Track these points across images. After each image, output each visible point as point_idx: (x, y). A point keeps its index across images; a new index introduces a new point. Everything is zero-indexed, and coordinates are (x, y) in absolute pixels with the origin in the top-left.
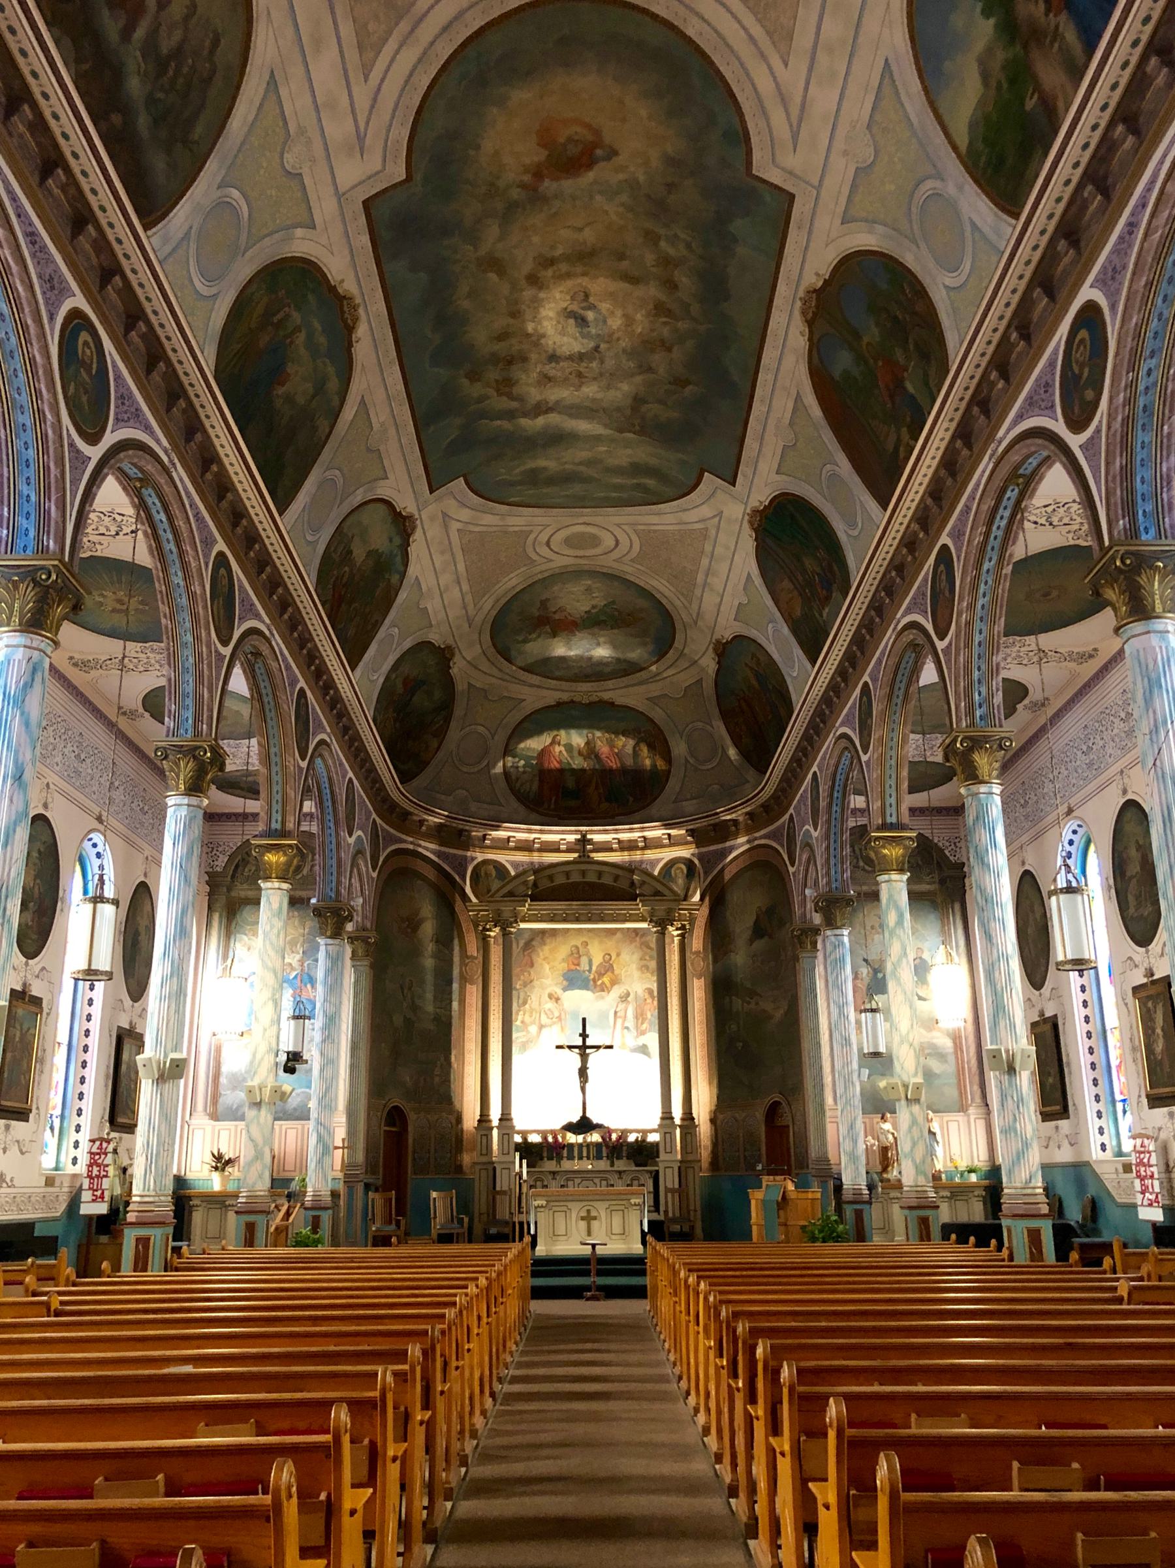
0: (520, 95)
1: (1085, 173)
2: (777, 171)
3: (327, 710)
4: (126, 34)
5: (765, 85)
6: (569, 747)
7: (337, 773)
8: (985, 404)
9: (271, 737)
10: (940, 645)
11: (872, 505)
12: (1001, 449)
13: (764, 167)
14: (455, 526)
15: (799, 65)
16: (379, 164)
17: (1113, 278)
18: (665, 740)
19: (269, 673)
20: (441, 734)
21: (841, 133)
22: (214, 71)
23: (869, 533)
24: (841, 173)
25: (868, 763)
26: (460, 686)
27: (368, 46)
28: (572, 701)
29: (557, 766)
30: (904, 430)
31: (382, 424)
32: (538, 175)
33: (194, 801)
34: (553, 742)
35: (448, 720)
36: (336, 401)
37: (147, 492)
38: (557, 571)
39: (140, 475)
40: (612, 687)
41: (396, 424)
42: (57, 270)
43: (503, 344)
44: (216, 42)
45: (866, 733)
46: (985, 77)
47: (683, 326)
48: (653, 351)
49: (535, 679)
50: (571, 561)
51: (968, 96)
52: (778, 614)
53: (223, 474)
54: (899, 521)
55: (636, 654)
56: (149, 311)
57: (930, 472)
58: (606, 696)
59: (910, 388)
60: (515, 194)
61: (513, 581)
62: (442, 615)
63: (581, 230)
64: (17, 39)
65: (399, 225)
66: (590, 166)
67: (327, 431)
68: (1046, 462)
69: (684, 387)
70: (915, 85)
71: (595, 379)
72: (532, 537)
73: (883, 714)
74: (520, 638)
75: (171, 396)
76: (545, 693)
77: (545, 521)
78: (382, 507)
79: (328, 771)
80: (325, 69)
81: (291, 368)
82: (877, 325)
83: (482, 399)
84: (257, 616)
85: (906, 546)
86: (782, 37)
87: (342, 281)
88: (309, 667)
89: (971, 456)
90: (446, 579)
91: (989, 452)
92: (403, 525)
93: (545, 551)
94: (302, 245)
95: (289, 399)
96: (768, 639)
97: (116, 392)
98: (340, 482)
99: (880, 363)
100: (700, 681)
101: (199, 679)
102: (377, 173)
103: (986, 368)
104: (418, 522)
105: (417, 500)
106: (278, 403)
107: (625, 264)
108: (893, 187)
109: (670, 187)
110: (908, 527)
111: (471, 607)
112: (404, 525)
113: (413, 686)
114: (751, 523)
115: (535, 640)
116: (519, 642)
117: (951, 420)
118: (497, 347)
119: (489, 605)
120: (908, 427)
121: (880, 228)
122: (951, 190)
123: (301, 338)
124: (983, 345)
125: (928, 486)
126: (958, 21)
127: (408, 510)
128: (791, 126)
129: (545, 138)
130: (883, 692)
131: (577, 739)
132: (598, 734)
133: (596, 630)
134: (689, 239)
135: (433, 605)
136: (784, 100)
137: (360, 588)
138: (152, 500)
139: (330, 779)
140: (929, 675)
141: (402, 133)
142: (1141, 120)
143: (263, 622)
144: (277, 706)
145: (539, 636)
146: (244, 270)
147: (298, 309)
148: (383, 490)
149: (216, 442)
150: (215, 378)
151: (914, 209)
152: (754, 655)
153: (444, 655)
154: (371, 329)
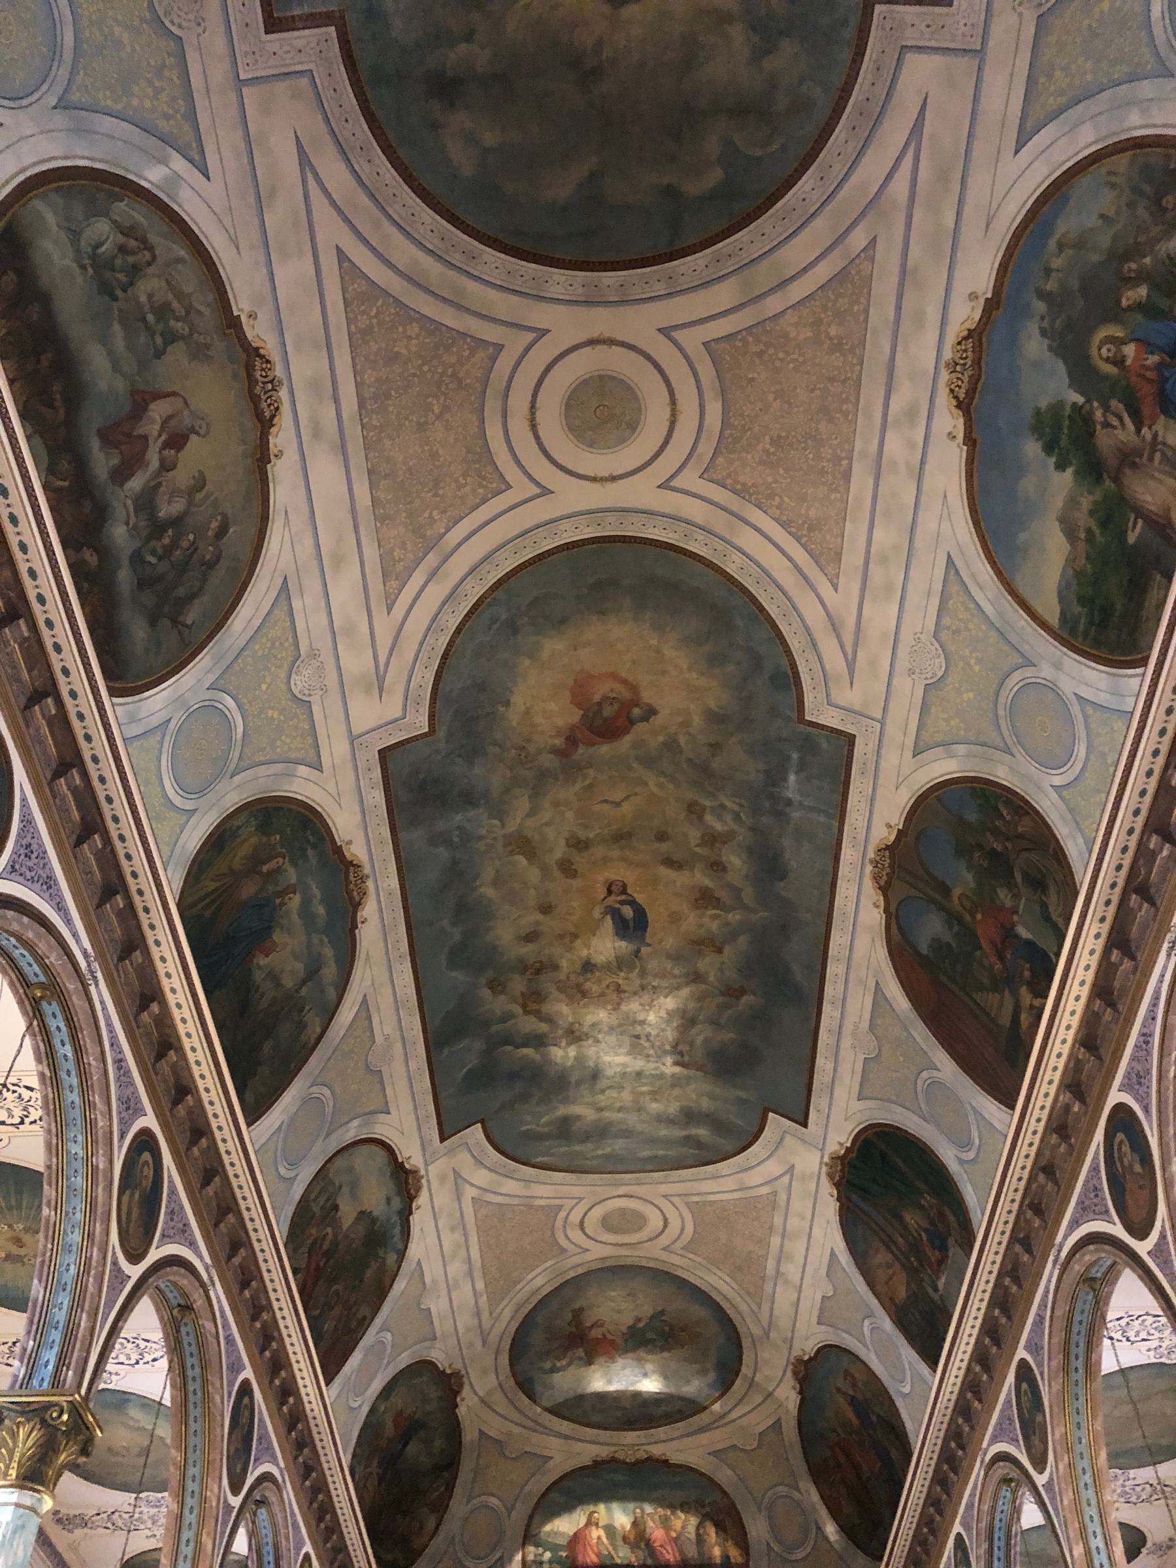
0: (553, 645)
1: (1011, 1237)
2: (835, 712)
3: (283, 1430)
4: (121, 475)
5: (813, 614)
6: (610, 1530)
7: (288, 1539)
8: (1027, 1242)
9: (190, 1450)
10: (1040, 1480)
11: (990, 1108)
12: (1064, 1254)
13: (819, 711)
14: (470, 1192)
15: (850, 585)
16: (395, 709)
17: (1140, 1084)
18: (738, 1513)
19: (200, 1336)
20: (440, 1507)
21: (903, 652)
22: (217, 559)
23: (989, 1147)
24: (908, 692)
25: (1049, 1486)
26: (469, 1435)
27: (394, 574)
28: (613, 1460)
29: (595, 1560)
30: (1024, 990)
31: (387, 1038)
32: (572, 740)
33: (28, 1498)
34: (589, 1523)
35: (450, 1487)
36: (332, 994)
37: (50, 1008)
38: (594, 1266)
39: (42, 979)
40: (663, 1437)
41: (403, 1038)
42: (135, 1092)
43: (531, 947)
44: (222, 531)
45: (1036, 1440)
46: (1070, 532)
47: (735, 917)
48: (700, 953)
49: (565, 1426)
50: (608, 1251)
51: (1051, 558)
52: (874, 1302)
53: (164, 1021)
54: (959, 1358)
55: (693, 1387)
56: (87, 757)
57: (1080, 1007)
58: (657, 1450)
59: (1023, 932)
60: (548, 761)
61: (539, 1280)
62: (449, 1326)
63: (618, 804)
64: (76, 702)
65: (417, 785)
66: (625, 731)
67: (318, 1030)
68: (1111, 1276)
69: (738, 998)
70: (985, 571)
71: (635, 993)
72: (562, 1214)
73: (1062, 1399)
74: (548, 1365)
75: (233, 1246)
76: (578, 1446)
77: (577, 1191)
78: (381, 1155)
79: (276, 1534)
80: (345, 590)
81: (277, 936)
82: (970, 867)
83: (507, 1017)
84: (274, 1461)
85: (1055, 1131)
86: (829, 559)
87: (350, 843)
88: (262, 1352)
89: (1136, 968)
90: (456, 1268)
91: (1051, 1258)
92: (404, 1182)
93: (576, 1235)
94: (303, 786)
95: (274, 977)
96: (866, 1346)
97: (167, 1207)
98: (329, 1108)
99: (979, 917)
100: (778, 1424)
101: (77, 1304)
102: (396, 720)
103: (1143, 833)
104: (424, 1181)
105: (423, 1149)
106: (258, 976)
107: (665, 847)
108: (971, 695)
109: (716, 747)
110: (1056, 1100)
111: (485, 1315)
112: (406, 1183)
113: (410, 1428)
114: (830, 1176)
115: (563, 1369)
116: (545, 1372)
117: (1102, 920)
118: (527, 950)
119: (506, 1319)
120: (1029, 984)
121: (961, 749)
122: (1046, 671)
123: (295, 901)
124: (1118, 854)
125: (1078, 1032)
126: (1028, 485)
127: (412, 1161)
128: (845, 655)
129: (580, 690)
130: (1054, 1363)
131: (620, 1517)
132: (649, 1509)
133: (641, 1353)
134: (736, 808)
135: (437, 1306)
136: (835, 627)
137: (346, 1262)
138: (56, 1023)
139: (276, 1547)
140: (1031, 1516)
141: (426, 678)
142: (1152, 890)
143: (278, 1465)
144: (207, 1398)
145: (569, 1365)
146: (232, 795)
147: (294, 863)
148: (383, 1129)
149: (290, 1350)
150: (178, 905)
151: (1001, 712)
152: (847, 1373)
153: (449, 1384)
154: (381, 910)
